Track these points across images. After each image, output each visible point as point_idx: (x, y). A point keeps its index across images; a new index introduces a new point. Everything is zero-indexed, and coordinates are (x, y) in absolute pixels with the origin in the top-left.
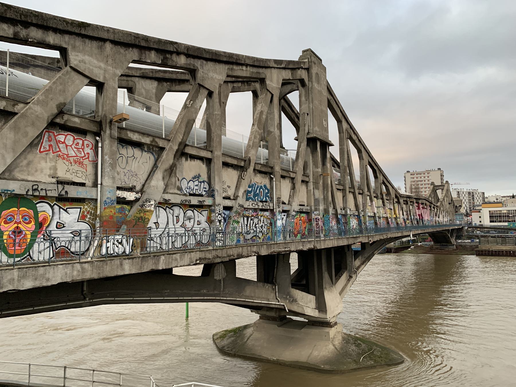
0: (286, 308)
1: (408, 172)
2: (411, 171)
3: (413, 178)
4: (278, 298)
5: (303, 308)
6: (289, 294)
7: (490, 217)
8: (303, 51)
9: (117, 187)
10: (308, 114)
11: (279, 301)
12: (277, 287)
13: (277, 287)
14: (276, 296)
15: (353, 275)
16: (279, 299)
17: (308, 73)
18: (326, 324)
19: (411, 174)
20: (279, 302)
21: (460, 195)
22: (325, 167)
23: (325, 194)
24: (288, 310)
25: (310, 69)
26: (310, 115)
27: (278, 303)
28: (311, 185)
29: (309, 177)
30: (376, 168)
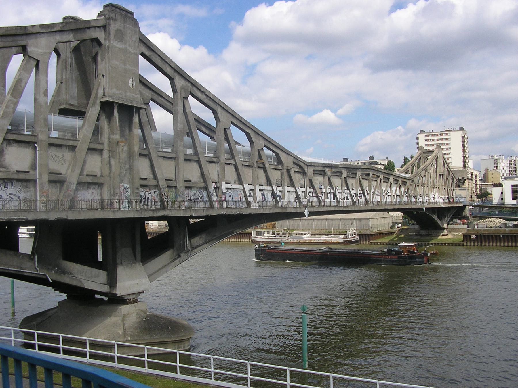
0: (49, 277)
1: (422, 132)
2: (427, 131)
3: (428, 140)
4: (37, 268)
5: (81, 282)
6: (57, 265)
7: (513, 192)
8: (63, 18)
9: (512, 185)
10: (103, 76)
11: (37, 270)
12: (36, 257)
13: (36, 257)
14: (35, 266)
15: (181, 255)
16: (38, 269)
17: (105, 31)
18: (121, 301)
19: (426, 136)
20: (37, 271)
21: (499, 165)
22: (131, 132)
23: (131, 163)
24: (51, 280)
25: (107, 27)
26: (106, 77)
27: (36, 273)
28: (106, 154)
29: (103, 144)
30: (248, 131)
